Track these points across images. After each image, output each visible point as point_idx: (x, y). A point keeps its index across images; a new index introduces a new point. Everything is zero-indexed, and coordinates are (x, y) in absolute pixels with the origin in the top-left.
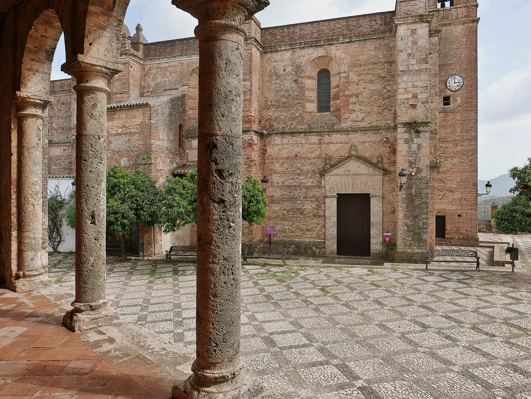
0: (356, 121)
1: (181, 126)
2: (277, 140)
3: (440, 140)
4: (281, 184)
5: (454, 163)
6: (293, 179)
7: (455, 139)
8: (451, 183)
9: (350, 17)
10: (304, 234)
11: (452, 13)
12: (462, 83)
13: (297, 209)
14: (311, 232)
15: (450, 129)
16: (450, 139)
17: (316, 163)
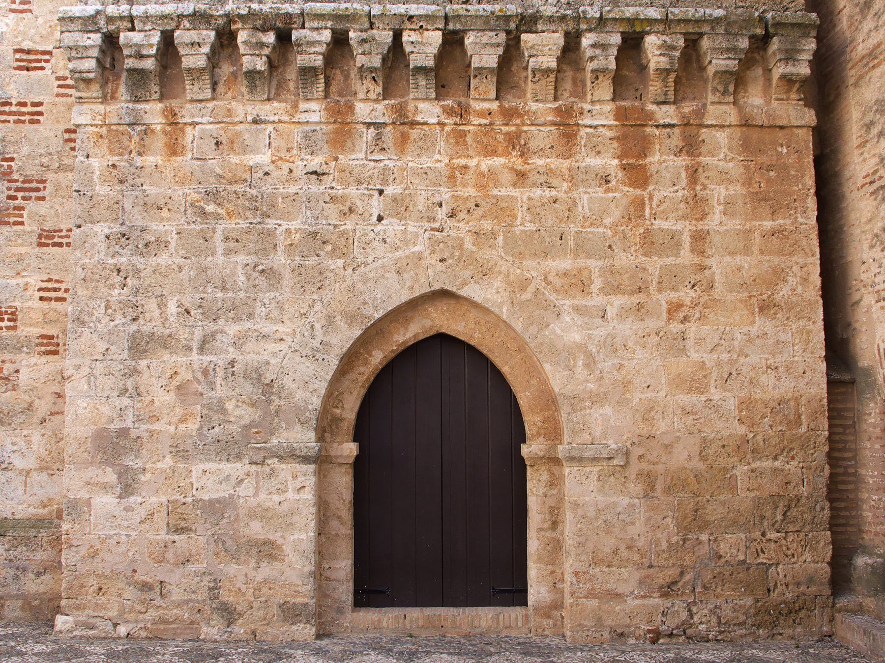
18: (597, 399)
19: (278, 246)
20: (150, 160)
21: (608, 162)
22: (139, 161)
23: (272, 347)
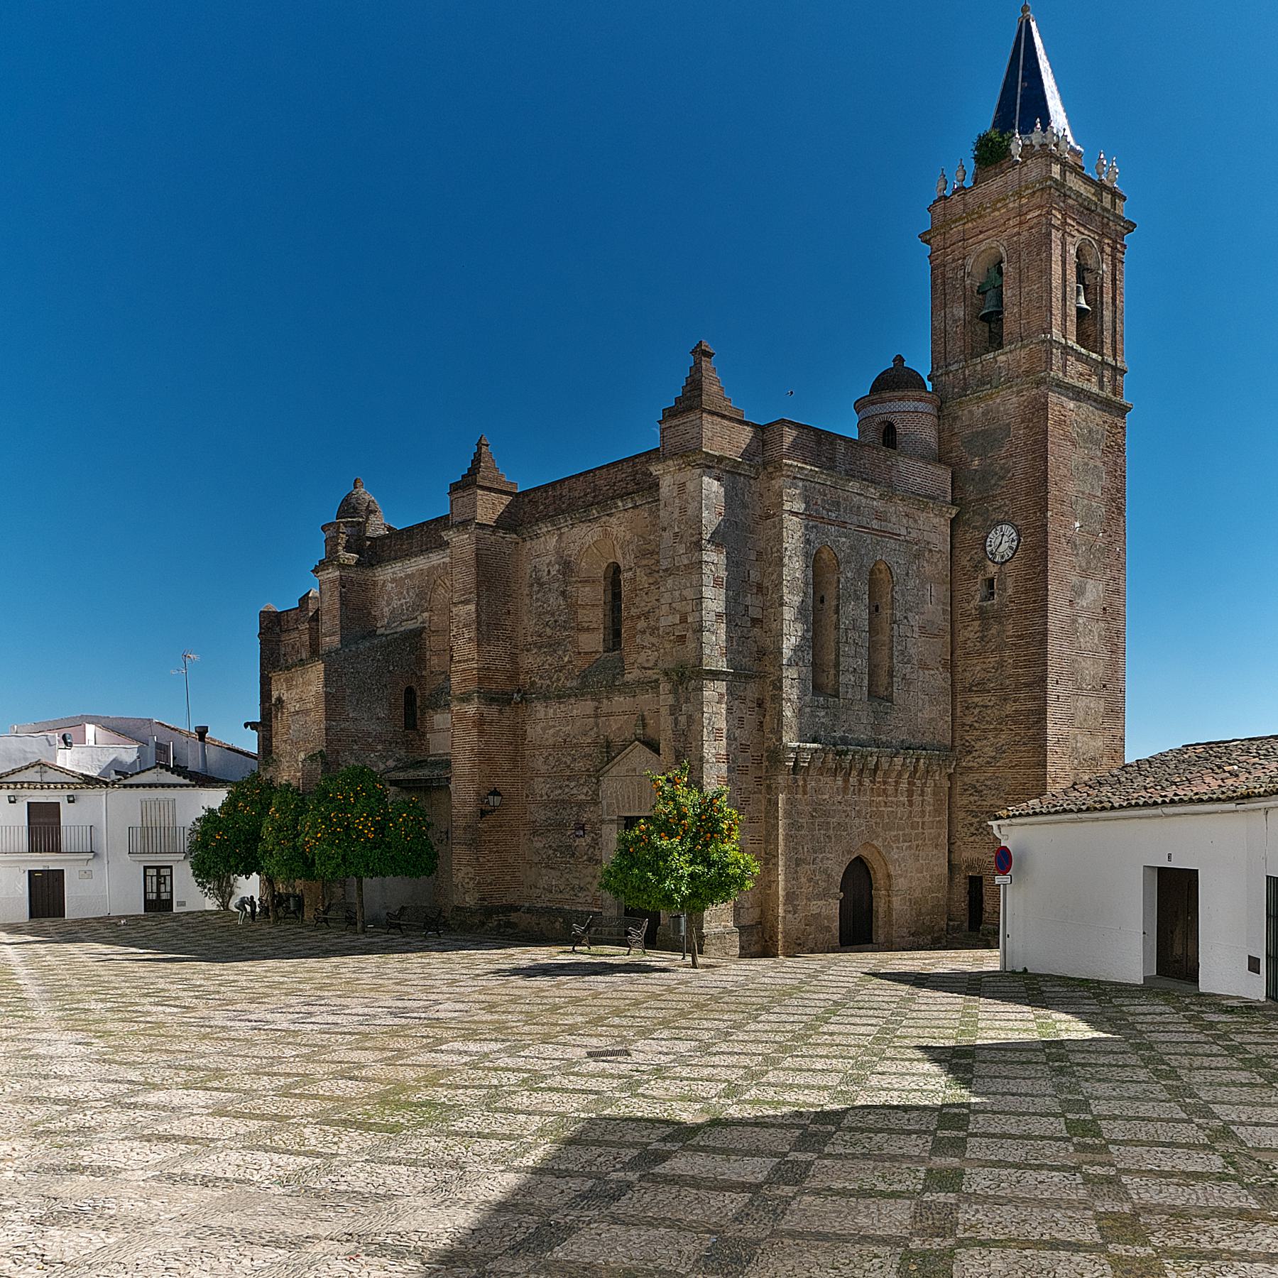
0: (645, 668)
1: (410, 692)
2: (540, 710)
3: (974, 688)
4: (545, 797)
5: (1000, 744)
6: (560, 788)
7: (1001, 685)
8: (993, 795)
9: (636, 456)
10: (575, 895)
11: (1000, 367)
12: (1016, 543)
13: (566, 846)
14: (585, 893)
15: (994, 659)
16: (992, 685)
17: (591, 755)
18: (901, 876)
19: (880, 607)
20: (799, 796)
21: (904, 799)
22: (796, 796)
23: (830, 862)
